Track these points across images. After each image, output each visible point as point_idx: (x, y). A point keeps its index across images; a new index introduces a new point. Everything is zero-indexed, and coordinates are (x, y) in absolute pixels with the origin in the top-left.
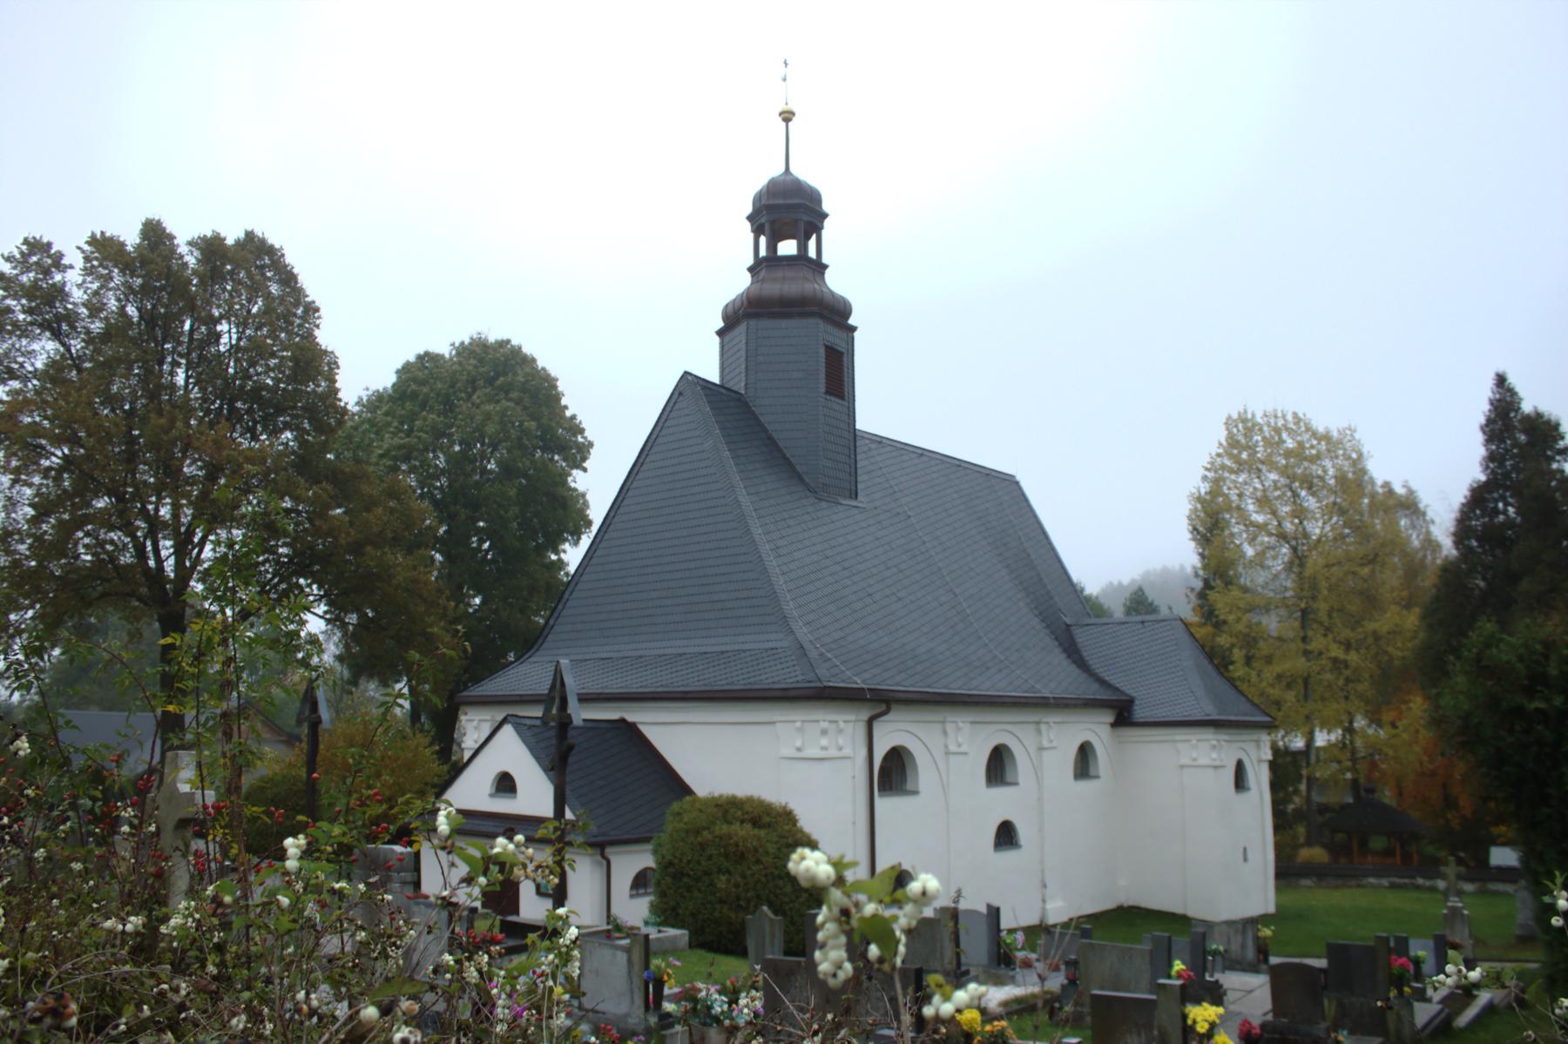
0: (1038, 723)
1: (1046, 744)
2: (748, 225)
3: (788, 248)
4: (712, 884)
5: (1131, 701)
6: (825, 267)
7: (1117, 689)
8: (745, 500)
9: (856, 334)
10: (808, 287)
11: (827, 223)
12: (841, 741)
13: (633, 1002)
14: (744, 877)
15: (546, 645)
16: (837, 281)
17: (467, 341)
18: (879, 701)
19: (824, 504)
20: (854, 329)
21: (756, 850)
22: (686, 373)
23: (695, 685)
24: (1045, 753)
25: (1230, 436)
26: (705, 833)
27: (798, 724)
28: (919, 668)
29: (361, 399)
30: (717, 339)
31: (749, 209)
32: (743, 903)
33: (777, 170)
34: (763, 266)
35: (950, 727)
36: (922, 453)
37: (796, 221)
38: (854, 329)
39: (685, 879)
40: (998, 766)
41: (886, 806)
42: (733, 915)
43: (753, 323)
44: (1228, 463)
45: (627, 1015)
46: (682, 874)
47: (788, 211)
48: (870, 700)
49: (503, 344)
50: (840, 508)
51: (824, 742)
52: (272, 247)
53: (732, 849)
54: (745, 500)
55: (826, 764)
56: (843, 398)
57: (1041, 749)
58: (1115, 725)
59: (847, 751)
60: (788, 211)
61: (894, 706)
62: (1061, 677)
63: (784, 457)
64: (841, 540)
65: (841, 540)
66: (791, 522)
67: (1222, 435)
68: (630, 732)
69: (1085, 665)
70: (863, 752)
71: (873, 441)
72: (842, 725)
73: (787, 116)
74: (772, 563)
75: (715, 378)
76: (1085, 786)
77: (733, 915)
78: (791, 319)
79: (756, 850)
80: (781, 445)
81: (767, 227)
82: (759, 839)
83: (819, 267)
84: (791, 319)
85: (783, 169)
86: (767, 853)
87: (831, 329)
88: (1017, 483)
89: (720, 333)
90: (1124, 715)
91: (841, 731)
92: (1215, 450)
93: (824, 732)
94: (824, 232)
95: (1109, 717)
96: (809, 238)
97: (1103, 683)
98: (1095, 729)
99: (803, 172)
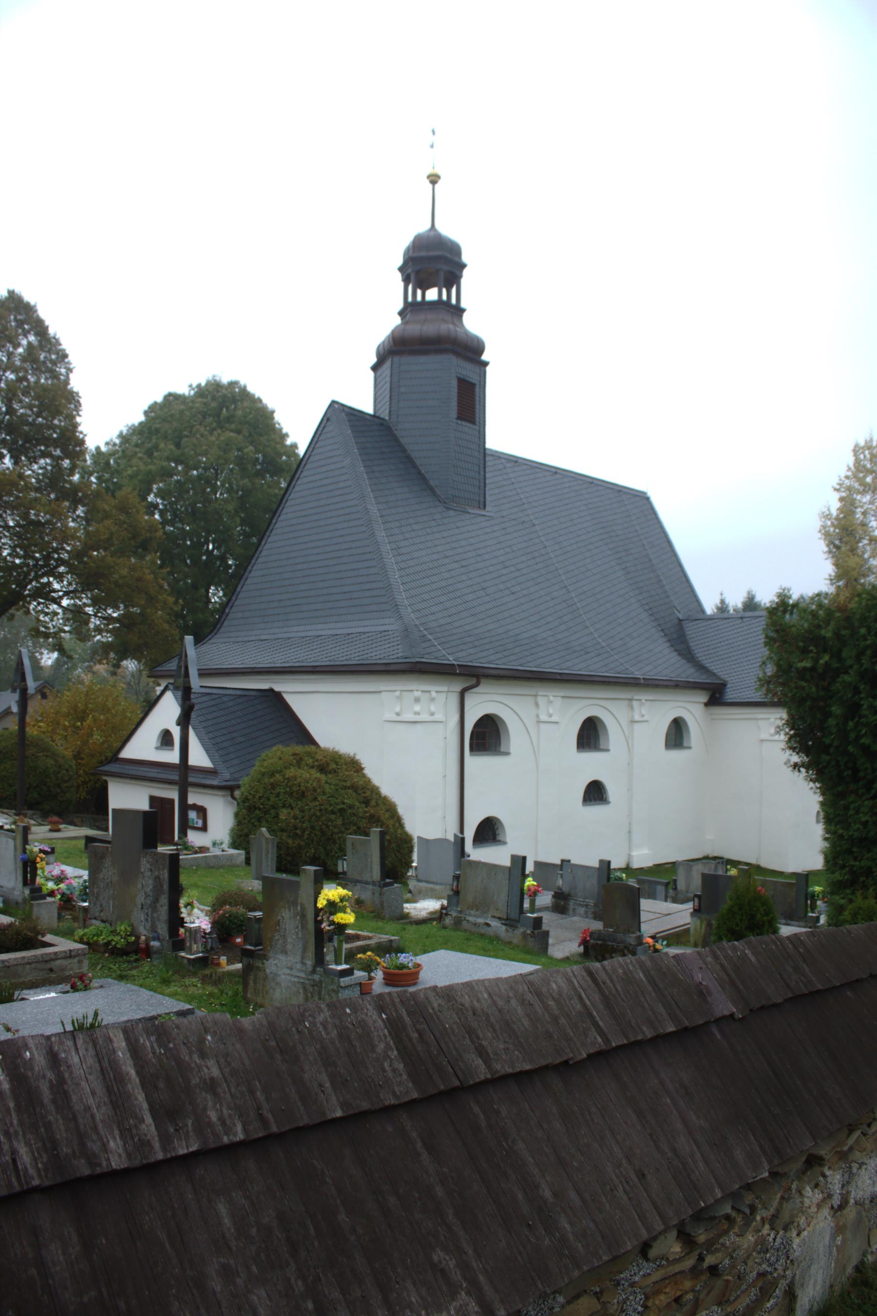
0: (631, 700)
1: (637, 717)
2: (399, 276)
3: (432, 294)
4: (277, 816)
5: (723, 685)
6: (463, 311)
7: (714, 674)
8: (374, 509)
9: (488, 369)
10: (444, 327)
11: (465, 272)
12: (433, 708)
13: (16, 878)
14: (303, 811)
15: (222, 630)
16: (473, 323)
17: (203, 384)
18: (471, 676)
19: (452, 513)
20: (486, 364)
21: (315, 790)
22: (333, 402)
23: (323, 661)
24: (636, 726)
25: (857, 461)
26: (277, 775)
27: (398, 693)
28: (517, 650)
29: (121, 433)
30: (372, 374)
31: (400, 262)
32: (298, 831)
33: (423, 227)
34: (410, 309)
35: (541, 701)
36: (556, 472)
37: (438, 271)
38: (486, 364)
39: (257, 812)
40: (590, 735)
41: (475, 763)
42: (290, 841)
43: (396, 359)
44: (856, 485)
45: (13, 889)
46: (255, 808)
47: (433, 263)
48: (460, 675)
49: (233, 384)
50: (467, 516)
51: (417, 708)
52: (28, 304)
53: (295, 789)
54: (374, 509)
55: (418, 726)
56: (474, 423)
57: (633, 722)
58: (707, 704)
59: (439, 717)
60: (433, 263)
61: (483, 681)
62: (666, 662)
63: (419, 473)
64: (463, 543)
65: (463, 543)
66: (416, 527)
67: (850, 460)
68: (276, 698)
69: (681, 650)
70: (456, 718)
71: (532, 467)
72: (434, 694)
73: (434, 179)
74: (390, 560)
75: (368, 407)
76: (676, 755)
77: (290, 841)
78: (434, 354)
79: (315, 790)
80: (418, 462)
81: (413, 277)
82: (319, 781)
83: (458, 311)
84: (434, 354)
85: (429, 226)
86: (324, 793)
87: (462, 363)
88: (648, 499)
89: (375, 368)
90: (716, 696)
91: (433, 699)
92: (843, 472)
93: (417, 700)
94: (463, 281)
95: (704, 698)
96: (452, 287)
97: (701, 668)
98: (690, 708)
99: (447, 229)
